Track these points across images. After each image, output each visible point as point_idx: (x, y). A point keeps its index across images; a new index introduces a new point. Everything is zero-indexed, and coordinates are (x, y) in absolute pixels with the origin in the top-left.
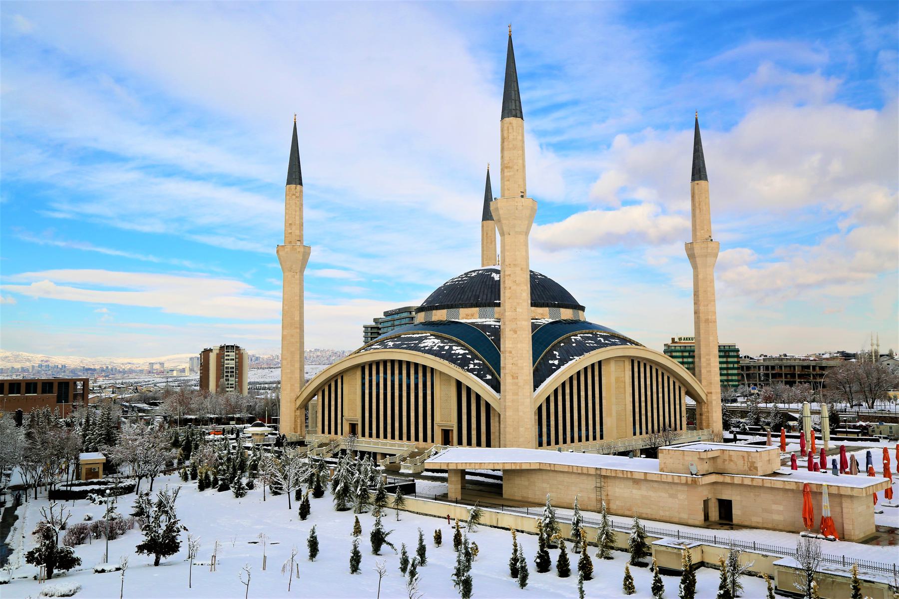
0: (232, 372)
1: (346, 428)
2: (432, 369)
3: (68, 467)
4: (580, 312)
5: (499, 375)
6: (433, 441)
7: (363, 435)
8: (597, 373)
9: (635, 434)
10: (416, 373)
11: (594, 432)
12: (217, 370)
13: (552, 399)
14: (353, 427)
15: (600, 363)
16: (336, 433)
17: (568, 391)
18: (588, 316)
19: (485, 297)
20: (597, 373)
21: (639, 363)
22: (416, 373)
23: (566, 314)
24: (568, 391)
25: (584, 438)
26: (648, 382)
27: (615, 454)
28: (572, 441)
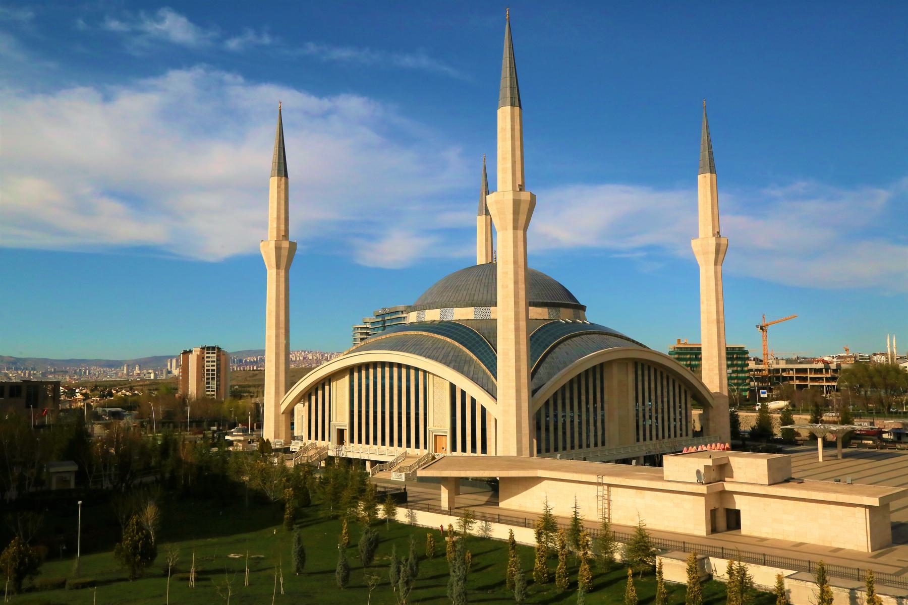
0: (213, 375)
1: (334, 435)
2: (425, 372)
3: (869, 434)
4: (581, 312)
5: (496, 378)
6: (425, 448)
7: (352, 441)
8: (598, 376)
9: (638, 440)
10: (649, 370)
11: (644, 435)
12: (496, 364)
13: (551, 403)
14: (341, 432)
15: (602, 365)
16: (316, 438)
17: (568, 395)
18: (592, 317)
19: (481, 296)
20: (598, 376)
21: (643, 365)
22: (649, 370)
23: (565, 316)
24: (568, 395)
25: (592, 444)
26: (653, 386)
27: (617, 462)
28: (572, 447)
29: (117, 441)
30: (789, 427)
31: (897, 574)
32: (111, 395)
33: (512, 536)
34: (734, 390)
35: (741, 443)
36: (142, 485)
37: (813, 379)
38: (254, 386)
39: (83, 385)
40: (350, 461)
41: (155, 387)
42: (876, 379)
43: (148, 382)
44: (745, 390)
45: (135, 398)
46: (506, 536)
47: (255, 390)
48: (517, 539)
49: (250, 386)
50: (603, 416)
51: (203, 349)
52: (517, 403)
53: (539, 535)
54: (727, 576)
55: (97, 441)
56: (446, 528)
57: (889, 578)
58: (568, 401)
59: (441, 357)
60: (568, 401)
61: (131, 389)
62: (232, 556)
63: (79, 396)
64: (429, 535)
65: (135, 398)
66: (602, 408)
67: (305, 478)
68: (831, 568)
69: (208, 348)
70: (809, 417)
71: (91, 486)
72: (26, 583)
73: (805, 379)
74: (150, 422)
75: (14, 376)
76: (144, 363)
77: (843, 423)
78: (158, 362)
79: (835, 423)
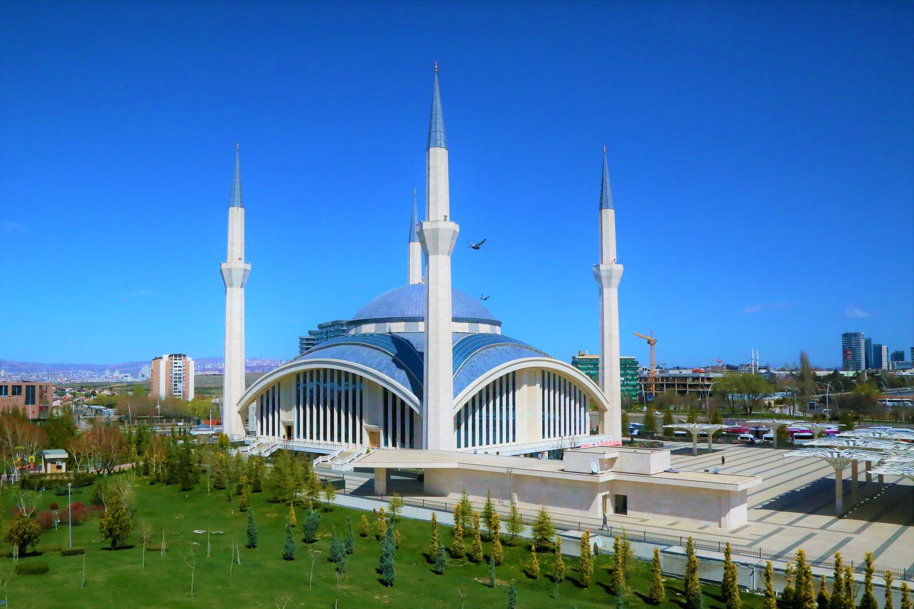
1: (283, 431)
13: (470, 405)
15: (514, 372)
29: (100, 435)
30: (670, 426)
31: (749, 546)
32: (94, 394)
33: (434, 519)
34: (625, 396)
35: (629, 439)
36: (121, 472)
37: (691, 386)
38: (215, 388)
39: (72, 386)
40: (296, 454)
41: (130, 388)
42: (743, 386)
43: (124, 384)
44: (635, 396)
45: (113, 398)
46: (430, 518)
47: (216, 392)
48: (438, 520)
49: (211, 388)
50: (514, 416)
51: (171, 356)
52: (888, 546)
53: (457, 519)
54: (614, 550)
55: (84, 433)
56: (378, 510)
57: (743, 549)
58: (343, 405)
59: (375, 365)
60: (343, 405)
61: (111, 389)
62: (196, 531)
63: (68, 395)
64: (363, 516)
65: (113, 398)
66: (514, 409)
67: (257, 467)
68: (698, 542)
69: (176, 355)
70: (686, 417)
71: (79, 471)
72: (29, 549)
73: (685, 386)
74: (127, 417)
75: (14, 379)
76: (122, 368)
77: (713, 423)
78: (134, 368)
79: (707, 423)
